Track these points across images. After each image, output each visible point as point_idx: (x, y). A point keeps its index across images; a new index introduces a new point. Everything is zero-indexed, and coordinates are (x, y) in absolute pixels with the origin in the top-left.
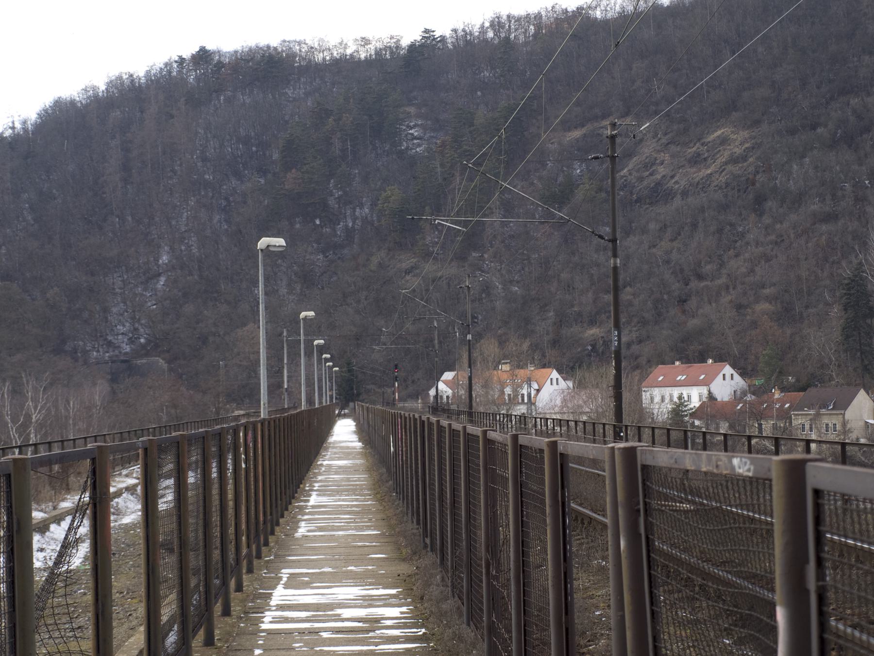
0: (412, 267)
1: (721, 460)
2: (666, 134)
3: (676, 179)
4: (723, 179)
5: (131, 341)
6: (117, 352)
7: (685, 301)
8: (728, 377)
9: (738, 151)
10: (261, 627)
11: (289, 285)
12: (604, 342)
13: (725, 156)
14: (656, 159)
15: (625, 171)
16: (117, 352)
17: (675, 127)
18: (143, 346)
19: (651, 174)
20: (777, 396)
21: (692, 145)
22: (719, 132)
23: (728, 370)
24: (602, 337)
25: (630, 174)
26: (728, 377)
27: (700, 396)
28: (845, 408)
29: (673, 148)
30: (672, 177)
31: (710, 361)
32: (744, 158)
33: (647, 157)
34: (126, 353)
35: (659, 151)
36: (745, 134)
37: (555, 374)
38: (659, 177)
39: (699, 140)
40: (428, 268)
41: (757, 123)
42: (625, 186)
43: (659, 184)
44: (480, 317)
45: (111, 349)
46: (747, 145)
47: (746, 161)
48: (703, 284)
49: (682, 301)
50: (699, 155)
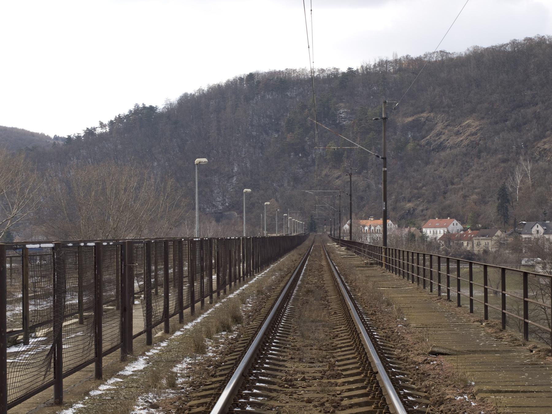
0: (339, 176)
2: (446, 121)
5: (222, 204)
7: (446, 193)
8: (455, 224)
9: (474, 130)
11: (288, 182)
14: (441, 132)
15: (428, 137)
18: (227, 207)
19: (439, 139)
21: (456, 126)
23: (455, 222)
25: (430, 138)
26: (455, 224)
30: (447, 140)
31: (437, 219)
32: (475, 134)
34: (220, 210)
35: (443, 129)
36: (477, 123)
39: (460, 124)
41: (483, 118)
46: (477, 128)
47: (477, 135)
48: (453, 186)
49: (445, 193)
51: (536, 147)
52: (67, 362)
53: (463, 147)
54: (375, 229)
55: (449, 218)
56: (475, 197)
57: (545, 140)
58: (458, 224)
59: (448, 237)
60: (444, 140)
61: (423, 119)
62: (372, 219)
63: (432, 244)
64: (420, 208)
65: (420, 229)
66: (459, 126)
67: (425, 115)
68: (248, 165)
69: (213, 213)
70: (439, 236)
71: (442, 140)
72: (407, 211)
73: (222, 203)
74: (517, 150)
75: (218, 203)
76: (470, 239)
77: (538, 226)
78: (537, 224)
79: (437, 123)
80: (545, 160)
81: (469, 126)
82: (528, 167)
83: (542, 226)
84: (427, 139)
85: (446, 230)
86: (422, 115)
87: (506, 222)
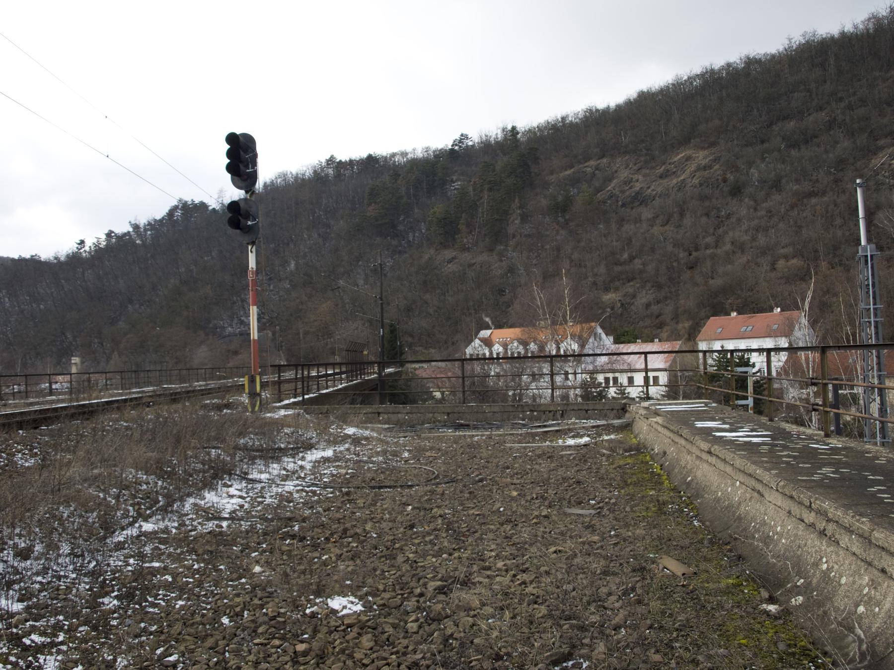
0: (453, 258)
2: (635, 164)
3: (652, 188)
4: (696, 181)
10: (252, 268)
12: (622, 305)
13: (693, 167)
17: (642, 159)
19: (631, 188)
24: (620, 300)
29: (645, 171)
36: (706, 152)
40: (466, 257)
42: (612, 197)
43: (638, 193)
44: (507, 291)
45: (242, 326)
50: (668, 171)
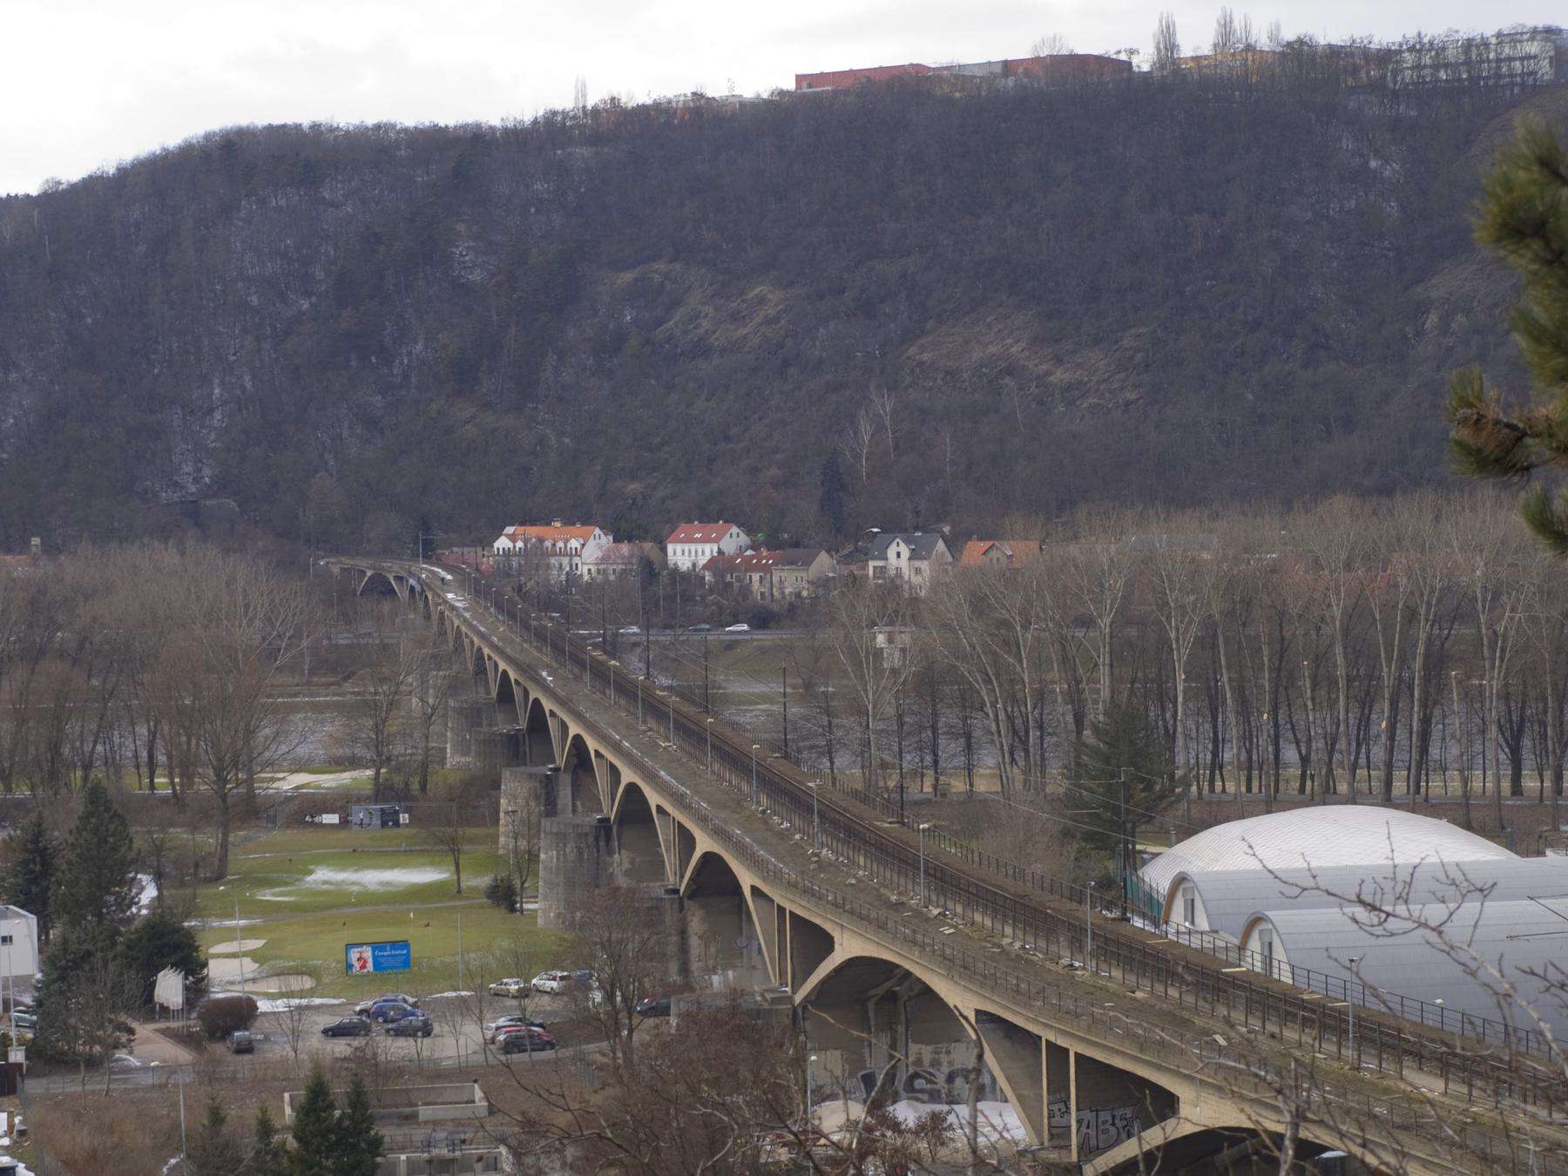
0: (471, 417)
1: (1143, 790)
2: (711, 285)
5: (196, 481)
6: (184, 493)
7: (714, 460)
8: (734, 535)
9: (772, 312)
11: (350, 428)
14: (700, 312)
15: (671, 323)
16: (184, 493)
18: (209, 486)
19: (695, 328)
20: (765, 554)
21: (734, 299)
22: (758, 290)
23: (735, 530)
25: (676, 326)
26: (734, 535)
27: (712, 552)
28: (809, 565)
30: (714, 332)
31: (696, 523)
32: (777, 320)
33: (692, 310)
34: (193, 494)
35: (704, 304)
36: (780, 294)
37: (597, 531)
38: (702, 331)
39: (741, 295)
41: (792, 283)
46: (780, 307)
47: (778, 322)
48: (729, 446)
49: (712, 460)
51: (905, 356)
52: (1481, 756)
53: (749, 353)
54: (566, 547)
55: (721, 522)
56: (774, 472)
57: (923, 341)
58: (742, 535)
59: (719, 564)
60: (707, 331)
61: (657, 276)
62: (558, 524)
63: (689, 579)
64: (660, 494)
65: (661, 542)
66: (739, 300)
67: (659, 266)
68: (248, 385)
69: (176, 503)
70: (702, 561)
71: (702, 331)
72: (631, 502)
73: (194, 479)
74: (864, 362)
75: (185, 477)
76: (767, 569)
77: (898, 544)
78: (898, 540)
79: (689, 288)
80: (923, 386)
81: (761, 300)
82: (884, 405)
83: (907, 542)
84: (669, 330)
85: (716, 549)
86: (656, 266)
87: (838, 530)
